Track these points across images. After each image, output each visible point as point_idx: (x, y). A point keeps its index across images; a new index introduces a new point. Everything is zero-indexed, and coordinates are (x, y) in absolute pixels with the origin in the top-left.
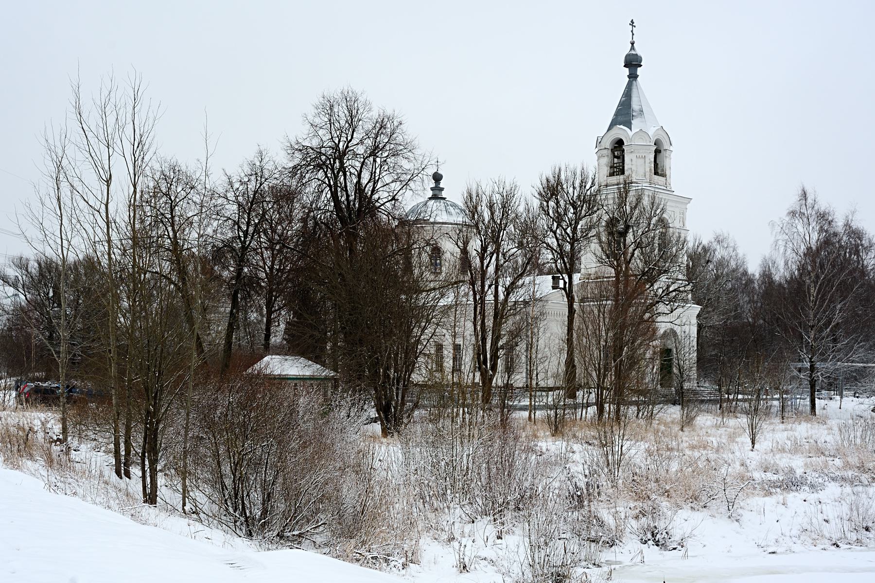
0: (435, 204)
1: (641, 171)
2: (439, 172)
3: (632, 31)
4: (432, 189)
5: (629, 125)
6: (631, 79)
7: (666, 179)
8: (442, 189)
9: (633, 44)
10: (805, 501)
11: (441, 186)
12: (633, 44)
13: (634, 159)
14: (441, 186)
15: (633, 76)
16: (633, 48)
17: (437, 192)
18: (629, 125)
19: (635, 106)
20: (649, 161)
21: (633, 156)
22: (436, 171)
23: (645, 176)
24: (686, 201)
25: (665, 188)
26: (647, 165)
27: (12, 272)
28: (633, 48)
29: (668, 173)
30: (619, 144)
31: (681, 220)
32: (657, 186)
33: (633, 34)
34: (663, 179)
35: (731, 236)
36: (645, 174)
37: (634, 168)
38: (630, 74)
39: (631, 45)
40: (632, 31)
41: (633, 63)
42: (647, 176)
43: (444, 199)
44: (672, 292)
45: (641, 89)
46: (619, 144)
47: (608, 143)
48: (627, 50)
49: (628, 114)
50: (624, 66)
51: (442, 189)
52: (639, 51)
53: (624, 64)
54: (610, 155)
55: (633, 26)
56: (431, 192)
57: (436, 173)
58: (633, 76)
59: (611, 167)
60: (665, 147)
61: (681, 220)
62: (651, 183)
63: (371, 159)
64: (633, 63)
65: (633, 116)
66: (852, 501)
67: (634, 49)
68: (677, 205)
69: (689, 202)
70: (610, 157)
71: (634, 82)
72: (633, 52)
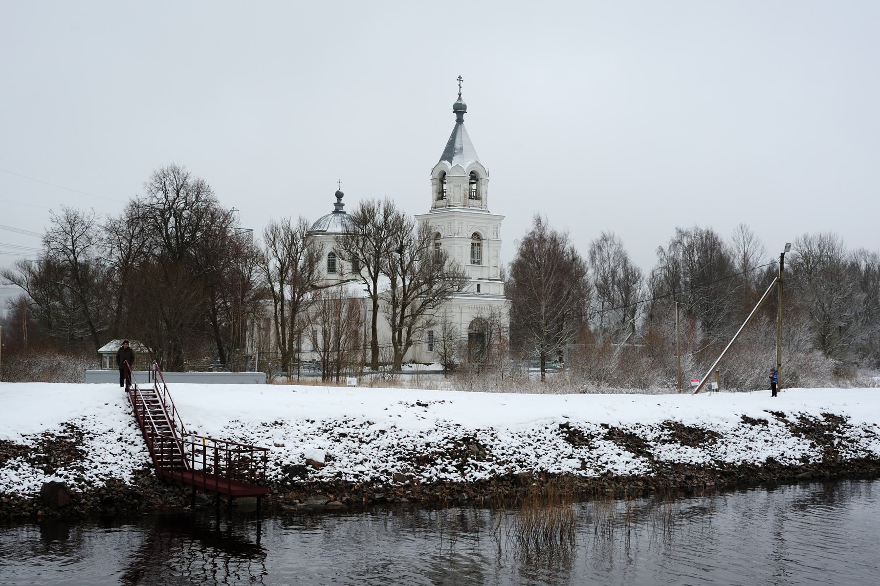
0: (333, 218)
1: (457, 197)
3: (459, 85)
4: (335, 204)
8: (343, 205)
9: (460, 95)
10: (659, 405)
11: (342, 202)
12: (460, 95)
14: (342, 202)
15: (460, 121)
16: (460, 98)
17: (338, 207)
18: (450, 160)
19: (457, 145)
25: (480, 209)
26: (462, 192)
27: (18, 274)
28: (460, 98)
29: (483, 197)
31: (495, 233)
33: (460, 87)
34: (479, 202)
37: (452, 194)
40: (459, 85)
41: (460, 110)
43: (344, 213)
47: (436, 175)
48: (455, 100)
51: (343, 205)
52: (465, 101)
55: (460, 80)
57: (338, 191)
58: (460, 121)
61: (495, 233)
63: (170, 198)
64: (460, 110)
66: (448, 542)
69: (503, 219)
71: (459, 125)
72: (459, 102)
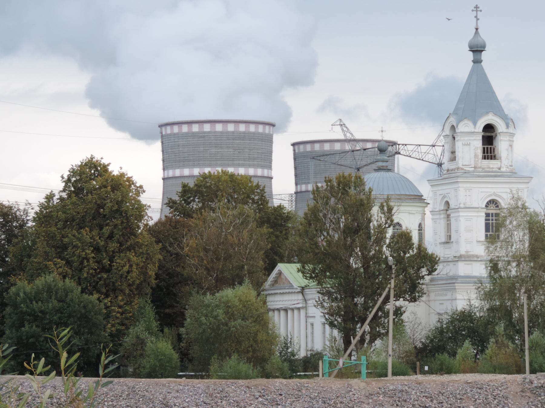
9: (477, 29)
12: (477, 29)
15: (477, 61)
33: (478, 19)
40: (476, 17)
55: (477, 11)
58: (477, 61)
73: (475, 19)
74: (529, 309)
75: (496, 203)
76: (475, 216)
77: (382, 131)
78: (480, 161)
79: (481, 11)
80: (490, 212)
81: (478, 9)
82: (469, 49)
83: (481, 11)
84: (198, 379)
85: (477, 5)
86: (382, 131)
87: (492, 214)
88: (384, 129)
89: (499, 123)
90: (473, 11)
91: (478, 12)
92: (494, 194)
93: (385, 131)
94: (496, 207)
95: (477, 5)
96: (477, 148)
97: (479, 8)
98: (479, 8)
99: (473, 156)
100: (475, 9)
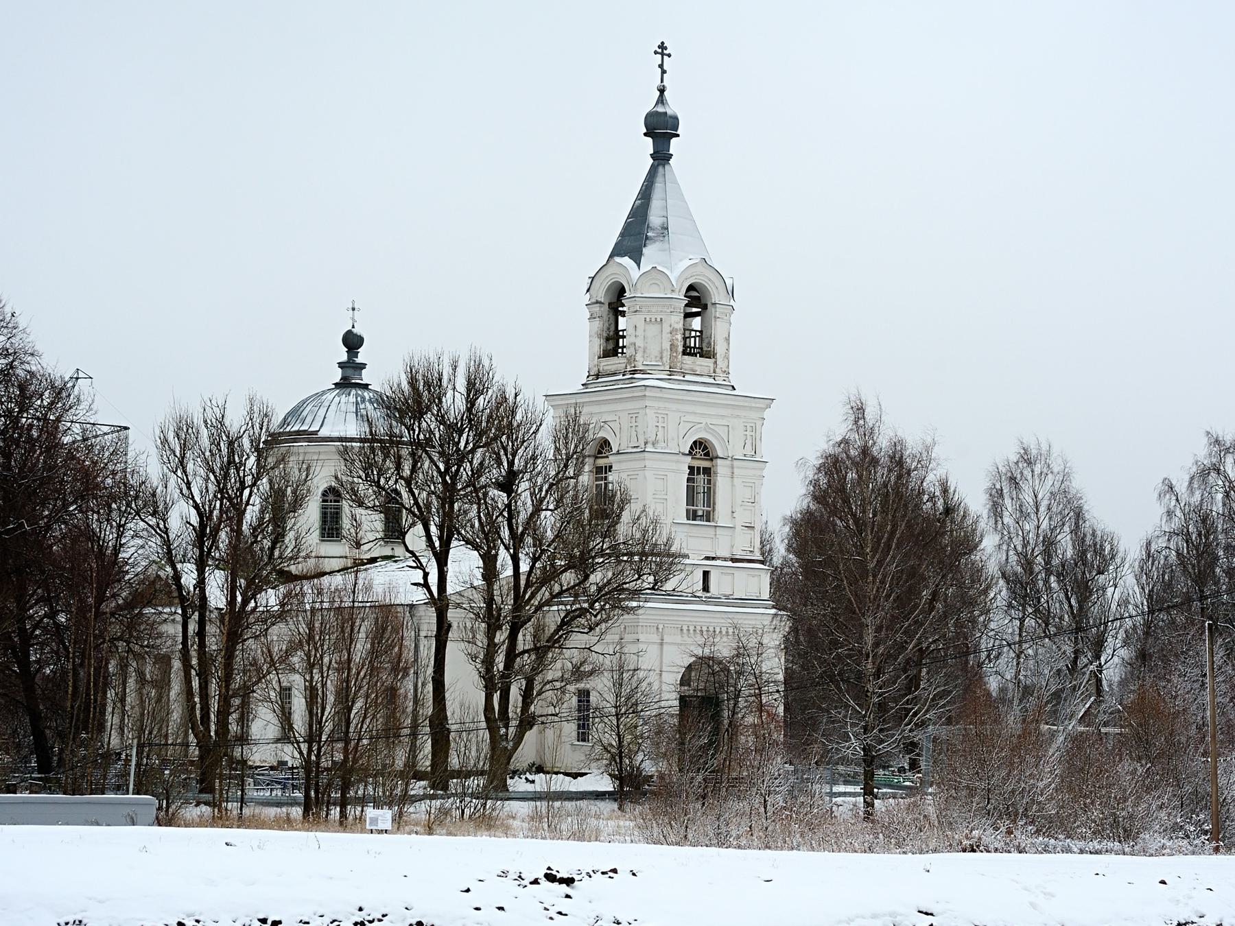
0: (337, 399)
2: (355, 331)
3: (661, 66)
5: (637, 258)
6: (656, 162)
7: (716, 362)
8: (362, 366)
9: (662, 91)
11: (360, 360)
12: (662, 91)
13: (641, 325)
14: (360, 360)
15: (661, 157)
16: (661, 100)
17: (349, 372)
18: (637, 258)
19: (654, 219)
20: (669, 329)
21: (638, 319)
22: (350, 328)
23: (661, 358)
24: (762, 404)
25: (711, 381)
28: (661, 100)
29: (720, 349)
30: (618, 294)
31: (749, 442)
32: (688, 378)
33: (664, 72)
34: (708, 362)
35: (1055, 451)
36: (661, 353)
37: (639, 343)
38: (654, 153)
39: (658, 93)
40: (661, 66)
42: (664, 359)
44: (165, 613)
45: (675, 182)
46: (618, 294)
47: (601, 293)
48: (649, 104)
49: (640, 234)
50: (645, 134)
52: (673, 106)
53: (645, 130)
54: (605, 315)
55: (663, 54)
56: (340, 370)
58: (661, 157)
59: (608, 339)
60: (715, 299)
61: (749, 442)
62: (671, 373)
65: (647, 238)
67: (662, 103)
68: (737, 412)
70: (605, 318)
71: (660, 169)
72: (660, 109)
73: (665, 68)
74: (138, 765)
75: (706, 448)
76: (673, 471)
77: (353, 309)
78: (680, 356)
79: (669, 55)
80: (696, 463)
81: (665, 52)
82: (645, 131)
83: (669, 55)
84: (572, 801)
85: (663, 43)
86: (353, 309)
87: (699, 468)
88: (356, 307)
89: (713, 283)
90: (656, 53)
91: (665, 57)
92: (707, 428)
93: (359, 310)
94: (705, 455)
95: (663, 43)
96: (676, 330)
97: (666, 48)
98: (666, 48)
99: (667, 345)
100: (660, 51)
